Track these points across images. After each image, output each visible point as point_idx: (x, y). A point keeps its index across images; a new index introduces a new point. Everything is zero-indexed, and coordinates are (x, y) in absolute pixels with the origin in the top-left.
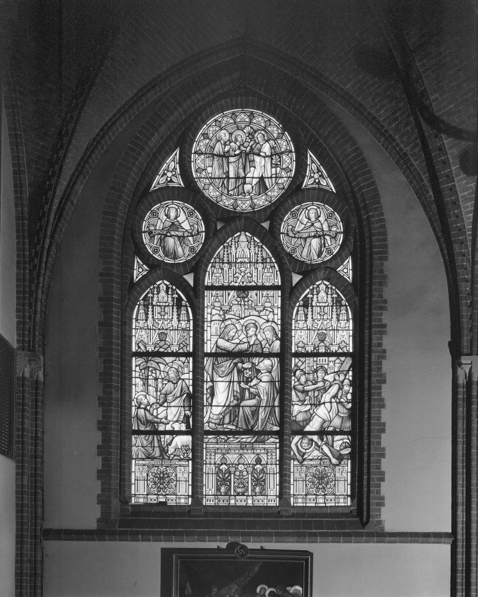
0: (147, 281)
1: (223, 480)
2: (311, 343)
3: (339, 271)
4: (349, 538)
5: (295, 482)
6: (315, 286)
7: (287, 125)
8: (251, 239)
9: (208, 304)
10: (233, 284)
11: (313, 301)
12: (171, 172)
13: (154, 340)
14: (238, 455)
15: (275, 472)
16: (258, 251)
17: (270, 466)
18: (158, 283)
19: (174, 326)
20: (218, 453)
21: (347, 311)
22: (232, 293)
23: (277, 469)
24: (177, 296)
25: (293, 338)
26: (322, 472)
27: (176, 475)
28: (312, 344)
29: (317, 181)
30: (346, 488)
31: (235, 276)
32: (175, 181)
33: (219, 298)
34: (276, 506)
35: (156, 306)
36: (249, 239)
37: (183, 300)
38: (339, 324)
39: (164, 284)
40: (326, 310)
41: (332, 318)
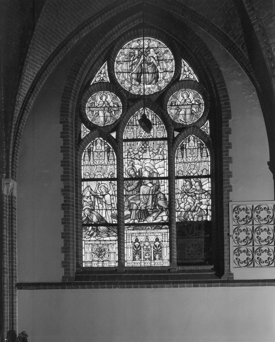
0: (90, 138)
1: (137, 252)
2: (93, 173)
3: (202, 129)
4: (264, 283)
5: (86, 254)
6: (95, 141)
7: (170, 45)
8: (149, 111)
9: (126, 150)
10: (139, 137)
11: (93, 149)
12: (103, 74)
13: (94, 171)
14: (145, 237)
15: (167, 246)
16: (154, 118)
17: (128, 243)
18: (96, 139)
19: (91, 164)
20: (134, 236)
21: (206, 151)
22: (139, 143)
23: (167, 244)
24: (107, 146)
25: (176, 168)
26: (101, 248)
27: (109, 250)
28: (93, 174)
29: (188, 76)
30: (115, 257)
31: (140, 133)
32: (105, 80)
33: (132, 146)
34: (168, 266)
35: (188, 149)
36: (148, 111)
37: (111, 148)
38: (202, 159)
39: (192, 136)
40: (194, 151)
41: (105, 158)
